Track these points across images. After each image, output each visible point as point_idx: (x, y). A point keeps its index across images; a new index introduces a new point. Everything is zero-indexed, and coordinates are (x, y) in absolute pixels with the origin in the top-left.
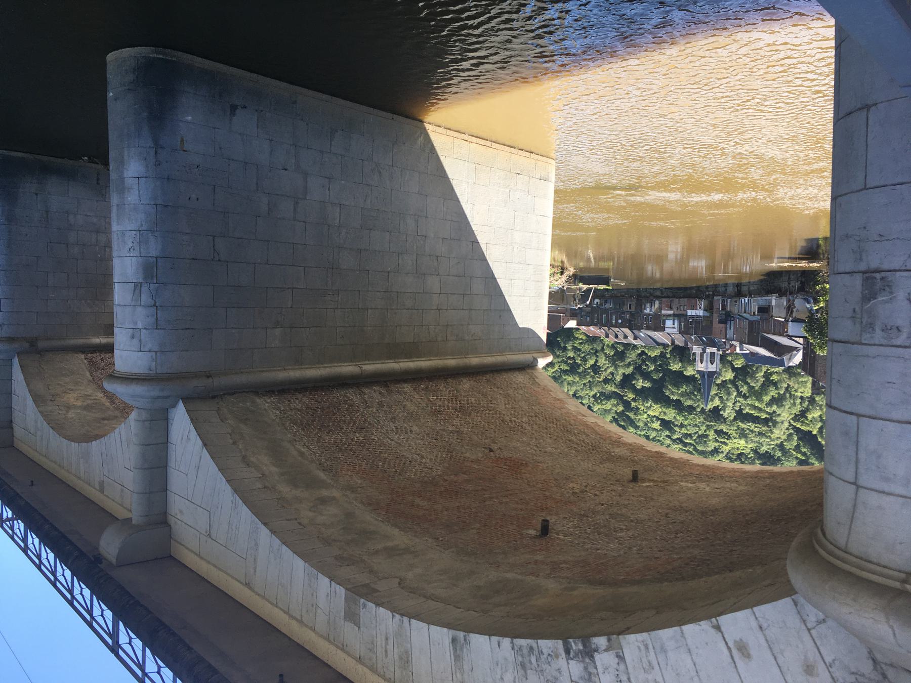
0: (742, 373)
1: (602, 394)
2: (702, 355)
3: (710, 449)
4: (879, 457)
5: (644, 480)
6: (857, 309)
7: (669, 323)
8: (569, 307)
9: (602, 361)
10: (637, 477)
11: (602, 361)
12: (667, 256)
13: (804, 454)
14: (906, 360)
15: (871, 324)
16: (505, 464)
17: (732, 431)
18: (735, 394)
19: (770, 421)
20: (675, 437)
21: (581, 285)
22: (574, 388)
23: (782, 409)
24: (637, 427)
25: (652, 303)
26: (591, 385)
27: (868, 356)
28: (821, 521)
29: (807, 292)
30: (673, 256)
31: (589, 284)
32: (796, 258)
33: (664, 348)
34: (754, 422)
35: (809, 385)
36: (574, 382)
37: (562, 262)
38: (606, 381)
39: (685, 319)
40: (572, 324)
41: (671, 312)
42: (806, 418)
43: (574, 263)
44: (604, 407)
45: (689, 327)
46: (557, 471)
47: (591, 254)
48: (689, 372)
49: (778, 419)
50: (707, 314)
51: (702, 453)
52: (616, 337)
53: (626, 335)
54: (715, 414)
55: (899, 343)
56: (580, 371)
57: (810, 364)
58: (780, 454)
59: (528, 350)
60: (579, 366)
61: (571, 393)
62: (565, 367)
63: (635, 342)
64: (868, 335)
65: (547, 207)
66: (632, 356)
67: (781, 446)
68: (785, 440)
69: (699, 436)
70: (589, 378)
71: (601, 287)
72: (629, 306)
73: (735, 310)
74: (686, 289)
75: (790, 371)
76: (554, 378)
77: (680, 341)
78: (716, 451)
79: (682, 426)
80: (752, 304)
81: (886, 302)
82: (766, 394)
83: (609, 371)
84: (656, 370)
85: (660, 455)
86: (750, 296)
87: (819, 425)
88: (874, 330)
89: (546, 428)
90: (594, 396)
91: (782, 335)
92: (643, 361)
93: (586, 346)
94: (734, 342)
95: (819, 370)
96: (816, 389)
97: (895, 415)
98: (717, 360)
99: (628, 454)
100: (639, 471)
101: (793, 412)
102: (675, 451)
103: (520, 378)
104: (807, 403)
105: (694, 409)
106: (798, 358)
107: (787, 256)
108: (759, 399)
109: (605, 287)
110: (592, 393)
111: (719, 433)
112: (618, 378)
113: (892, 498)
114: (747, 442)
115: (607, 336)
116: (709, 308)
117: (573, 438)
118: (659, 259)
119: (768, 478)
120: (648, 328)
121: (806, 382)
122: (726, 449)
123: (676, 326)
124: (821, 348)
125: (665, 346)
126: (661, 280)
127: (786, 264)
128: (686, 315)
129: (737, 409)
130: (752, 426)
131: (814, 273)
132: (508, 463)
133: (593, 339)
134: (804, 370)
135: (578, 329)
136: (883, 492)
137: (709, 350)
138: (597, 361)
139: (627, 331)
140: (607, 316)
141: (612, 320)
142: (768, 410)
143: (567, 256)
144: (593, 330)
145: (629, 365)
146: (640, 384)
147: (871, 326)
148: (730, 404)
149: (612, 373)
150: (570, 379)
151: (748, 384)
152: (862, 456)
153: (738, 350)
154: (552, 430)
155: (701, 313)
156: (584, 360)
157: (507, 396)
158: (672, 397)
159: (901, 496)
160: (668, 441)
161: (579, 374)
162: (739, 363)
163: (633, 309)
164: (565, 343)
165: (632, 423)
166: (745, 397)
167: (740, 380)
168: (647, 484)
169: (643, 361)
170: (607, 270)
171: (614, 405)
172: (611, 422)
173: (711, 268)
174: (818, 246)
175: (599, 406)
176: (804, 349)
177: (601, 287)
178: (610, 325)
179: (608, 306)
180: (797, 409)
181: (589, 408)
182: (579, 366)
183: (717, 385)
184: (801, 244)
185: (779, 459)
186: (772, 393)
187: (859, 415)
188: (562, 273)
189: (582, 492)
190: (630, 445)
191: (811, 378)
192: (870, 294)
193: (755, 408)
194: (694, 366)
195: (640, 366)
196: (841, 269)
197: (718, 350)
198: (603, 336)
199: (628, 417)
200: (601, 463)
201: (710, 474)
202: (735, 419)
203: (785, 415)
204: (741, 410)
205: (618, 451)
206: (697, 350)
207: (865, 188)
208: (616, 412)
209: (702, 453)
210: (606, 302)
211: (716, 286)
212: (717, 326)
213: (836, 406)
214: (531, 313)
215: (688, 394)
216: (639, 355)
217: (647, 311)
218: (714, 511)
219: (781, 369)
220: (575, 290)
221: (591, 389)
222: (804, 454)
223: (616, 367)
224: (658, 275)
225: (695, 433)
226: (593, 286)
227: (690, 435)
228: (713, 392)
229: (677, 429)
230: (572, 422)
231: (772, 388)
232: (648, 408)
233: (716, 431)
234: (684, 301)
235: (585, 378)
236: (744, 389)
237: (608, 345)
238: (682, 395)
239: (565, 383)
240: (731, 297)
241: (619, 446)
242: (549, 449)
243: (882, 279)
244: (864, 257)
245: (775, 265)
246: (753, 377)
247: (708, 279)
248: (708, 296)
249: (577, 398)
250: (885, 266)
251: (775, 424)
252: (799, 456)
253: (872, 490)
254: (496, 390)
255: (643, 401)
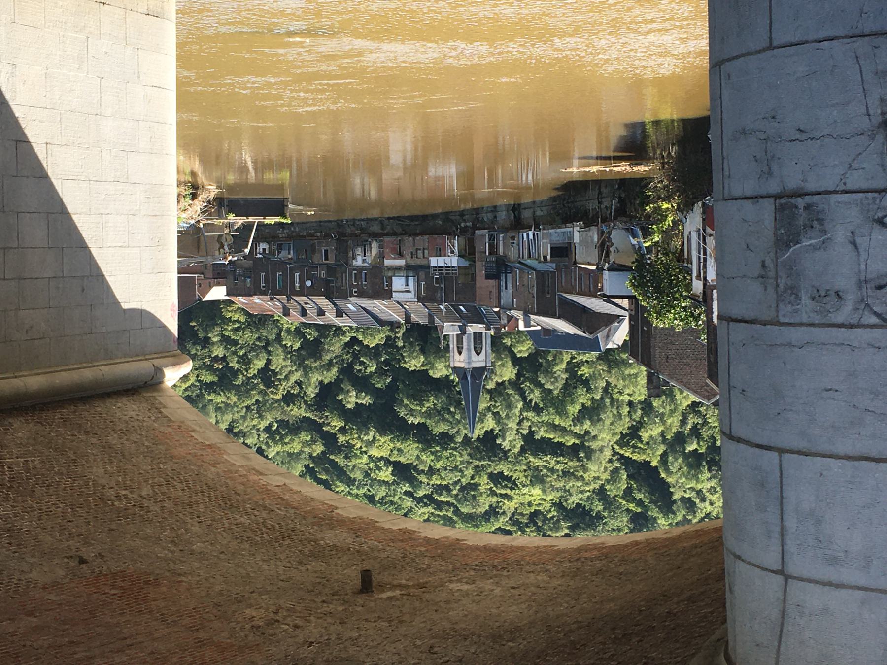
0: (531, 367)
1: (282, 423)
2: (459, 339)
3: (482, 510)
4: (818, 522)
5: (382, 587)
6: (768, 262)
7: (398, 283)
8: (210, 260)
9: (279, 362)
10: (370, 582)
11: (279, 362)
12: (388, 158)
13: (640, 503)
14: (853, 349)
15: (792, 288)
16: (113, 586)
17: (519, 475)
18: (520, 405)
19: (580, 450)
20: (420, 493)
21: (231, 217)
22: (228, 417)
23: (599, 426)
24: (350, 482)
25: (365, 246)
26: (260, 408)
27: (790, 345)
28: (723, 641)
29: (631, 218)
30: (397, 159)
31: (247, 216)
32: (608, 158)
33: (392, 330)
34: (554, 454)
35: (643, 381)
36: (227, 405)
37: (193, 174)
38: (289, 399)
39: (427, 274)
40: (218, 293)
41: (401, 262)
42: (639, 438)
43: (216, 174)
44: (287, 448)
45: (434, 288)
46: (218, 588)
47: (248, 159)
48: (439, 371)
49: (594, 445)
50: (465, 263)
51: (469, 518)
52: (304, 313)
53: (321, 309)
54: (489, 445)
55: (840, 318)
56: (239, 381)
57: (641, 345)
58: (600, 508)
59: (142, 354)
60: (235, 373)
61: (224, 426)
62: (209, 378)
63: (338, 322)
64: (789, 308)
65: (165, 70)
66: (335, 347)
67: (601, 493)
68: (608, 481)
69: (463, 488)
70: (256, 396)
71: (271, 220)
72: (325, 254)
73: (513, 254)
74: (424, 218)
75: (609, 358)
76: (188, 399)
77: (420, 316)
78: (493, 512)
79: (431, 471)
80: (539, 242)
81: (815, 248)
82: (573, 402)
83: (294, 378)
84: (380, 372)
85: (407, 536)
86: (537, 227)
87: (662, 449)
88: (798, 298)
89: (191, 506)
90: (268, 429)
91: (594, 296)
92: (356, 356)
93: (248, 334)
94: (513, 313)
95: (657, 353)
96: (655, 387)
97: (843, 447)
98: (487, 344)
99: (349, 540)
100: (373, 575)
101: (618, 430)
102: (420, 521)
103: (128, 410)
104: (639, 412)
105: (451, 438)
106: (621, 334)
107: (594, 154)
108: (561, 412)
109: (278, 219)
110: (263, 425)
111: (497, 478)
112: (312, 392)
113: (843, 592)
114: (544, 491)
115: (286, 313)
116: (468, 252)
117: (244, 520)
118: (375, 163)
119: (598, 558)
120: (361, 294)
121: (636, 376)
122: (509, 506)
123: (412, 287)
124: (659, 314)
125: (393, 325)
126: (379, 203)
127: (595, 169)
128: (428, 267)
129: (525, 432)
130: (551, 461)
131: (638, 184)
132: (120, 583)
133: (258, 321)
134: (633, 354)
135: (229, 303)
136: (830, 584)
137: (472, 328)
138: (269, 362)
139: (322, 301)
140: (285, 275)
141: (293, 282)
142: (577, 429)
143: (202, 161)
144: (259, 303)
145: (330, 364)
146: (352, 399)
147: (794, 290)
148: (512, 424)
149: (299, 383)
150: (220, 399)
151: (540, 385)
152: (791, 523)
153: (522, 327)
154: (201, 508)
155: (453, 261)
156: (245, 361)
157: (107, 448)
158: (411, 420)
159: (860, 588)
160: (409, 503)
161: (237, 388)
162: (523, 349)
163: (331, 261)
164: (206, 332)
165: (341, 474)
166: (537, 410)
167: (526, 379)
168: (389, 594)
169: (356, 356)
170: (281, 187)
171: (306, 444)
172: (302, 475)
173: (467, 178)
174: (645, 135)
175: (279, 448)
176: (631, 318)
177: (271, 220)
178: (291, 293)
179: (284, 255)
180: (624, 425)
181: (260, 451)
182: (235, 373)
183: (489, 391)
184: (617, 133)
185: (599, 517)
186: (582, 400)
187: (781, 451)
188: (194, 196)
189: (271, 623)
190: (352, 521)
191: (644, 368)
192: (786, 239)
193: (555, 427)
194: (447, 359)
195: (351, 365)
196: (737, 193)
197: (488, 329)
198: (278, 314)
199: (334, 464)
200: (300, 563)
201: (495, 563)
202: (523, 450)
203: (605, 436)
204: (531, 433)
205: (329, 537)
206: (450, 329)
207: (771, 47)
208: (311, 456)
209: (469, 518)
210: (280, 248)
211: (477, 211)
212: (483, 284)
213: (743, 436)
214: (144, 277)
215: (439, 412)
216: (348, 345)
217: (358, 262)
218: (514, 632)
219: (593, 355)
220: (220, 228)
221: (261, 417)
222: (640, 503)
223: (307, 370)
224: (373, 194)
225: (456, 483)
226: (255, 220)
227: (447, 488)
228: (482, 406)
229: (423, 478)
230: (240, 488)
231: (581, 391)
232: (370, 444)
233: (491, 476)
234: (423, 241)
235: (249, 396)
236: (535, 396)
237: (288, 331)
238: (428, 414)
239: (211, 408)
240: (504, 230)
241: (332, 527)
242: (198, 546)
243: (808, 207)
244: (775, 167)
245: (575, 170)
246: (549, 373)
247: (463, 199)
248: (464, 231)
249: (236, 435)
250: (811, 186)
251: (589, 453)
252: (632, 506)
253: (810, 581)
254: (83, 437)
255: (360, 431)
